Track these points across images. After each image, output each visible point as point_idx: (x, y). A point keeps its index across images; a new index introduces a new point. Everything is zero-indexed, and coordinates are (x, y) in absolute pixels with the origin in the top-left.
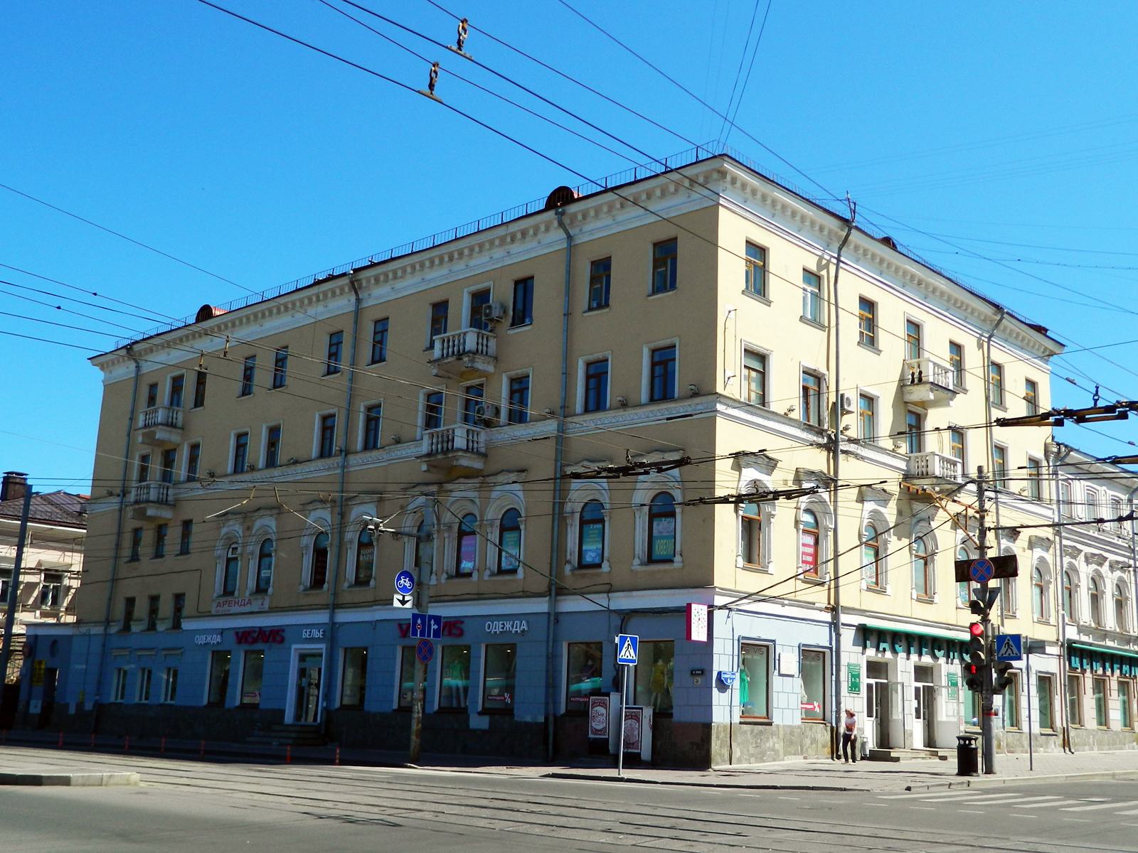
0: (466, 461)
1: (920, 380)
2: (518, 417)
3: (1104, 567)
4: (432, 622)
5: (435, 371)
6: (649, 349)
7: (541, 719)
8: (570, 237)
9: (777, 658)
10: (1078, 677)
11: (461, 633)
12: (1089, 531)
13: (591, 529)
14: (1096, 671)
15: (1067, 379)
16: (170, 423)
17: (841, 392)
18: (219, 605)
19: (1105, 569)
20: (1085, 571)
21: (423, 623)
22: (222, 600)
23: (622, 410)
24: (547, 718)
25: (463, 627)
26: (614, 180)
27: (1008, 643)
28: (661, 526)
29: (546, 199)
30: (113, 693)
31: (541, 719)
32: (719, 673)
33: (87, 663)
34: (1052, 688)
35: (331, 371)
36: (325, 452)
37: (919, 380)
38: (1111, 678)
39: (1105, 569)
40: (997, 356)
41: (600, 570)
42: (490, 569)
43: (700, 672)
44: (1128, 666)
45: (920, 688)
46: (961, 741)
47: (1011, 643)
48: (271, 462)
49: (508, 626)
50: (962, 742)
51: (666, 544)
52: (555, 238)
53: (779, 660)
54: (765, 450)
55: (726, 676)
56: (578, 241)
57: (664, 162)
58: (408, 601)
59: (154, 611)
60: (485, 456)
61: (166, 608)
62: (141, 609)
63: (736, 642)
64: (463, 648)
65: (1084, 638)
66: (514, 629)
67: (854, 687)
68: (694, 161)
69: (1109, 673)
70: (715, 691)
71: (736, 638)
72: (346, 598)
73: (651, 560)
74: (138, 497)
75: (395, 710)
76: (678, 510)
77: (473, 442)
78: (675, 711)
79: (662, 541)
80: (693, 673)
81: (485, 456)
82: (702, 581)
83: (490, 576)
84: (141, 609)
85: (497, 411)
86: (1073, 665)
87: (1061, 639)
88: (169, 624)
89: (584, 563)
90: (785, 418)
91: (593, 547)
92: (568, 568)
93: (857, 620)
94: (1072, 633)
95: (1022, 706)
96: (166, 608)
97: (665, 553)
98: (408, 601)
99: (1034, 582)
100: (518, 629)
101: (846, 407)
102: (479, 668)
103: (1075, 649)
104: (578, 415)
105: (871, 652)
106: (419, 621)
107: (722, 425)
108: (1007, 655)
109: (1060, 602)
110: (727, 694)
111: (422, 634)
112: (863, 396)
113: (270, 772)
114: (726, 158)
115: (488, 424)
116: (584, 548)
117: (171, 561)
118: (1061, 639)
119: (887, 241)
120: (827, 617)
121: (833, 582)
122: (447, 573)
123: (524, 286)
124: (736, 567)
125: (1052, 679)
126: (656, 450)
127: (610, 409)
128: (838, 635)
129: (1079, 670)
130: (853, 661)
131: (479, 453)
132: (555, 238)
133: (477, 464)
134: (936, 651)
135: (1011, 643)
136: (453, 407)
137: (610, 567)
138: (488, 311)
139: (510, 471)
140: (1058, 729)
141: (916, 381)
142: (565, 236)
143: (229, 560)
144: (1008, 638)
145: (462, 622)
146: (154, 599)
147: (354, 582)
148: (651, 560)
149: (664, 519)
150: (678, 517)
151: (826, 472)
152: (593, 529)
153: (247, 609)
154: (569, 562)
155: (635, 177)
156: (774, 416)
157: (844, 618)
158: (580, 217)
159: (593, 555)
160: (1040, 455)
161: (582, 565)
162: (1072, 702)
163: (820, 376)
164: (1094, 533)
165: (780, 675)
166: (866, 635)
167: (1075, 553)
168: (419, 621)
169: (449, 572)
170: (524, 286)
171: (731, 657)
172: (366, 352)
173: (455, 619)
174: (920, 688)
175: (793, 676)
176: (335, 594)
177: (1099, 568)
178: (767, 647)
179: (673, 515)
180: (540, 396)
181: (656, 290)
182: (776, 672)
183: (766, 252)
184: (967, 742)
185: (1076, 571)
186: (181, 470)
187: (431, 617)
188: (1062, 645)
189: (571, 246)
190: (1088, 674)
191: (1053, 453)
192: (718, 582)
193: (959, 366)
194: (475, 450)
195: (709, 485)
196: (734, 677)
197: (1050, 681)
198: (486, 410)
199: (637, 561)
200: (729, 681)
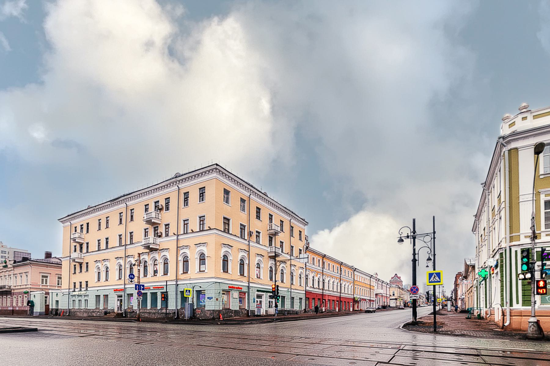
2: (167, 235)
4: (141, 286)
20: (310, 277)
21: (139, 287)
36: (120, 245)
48: (107, 248)
59: (81, 286)
61: (84, 285)
62: (78, 286)
76: (206, 258)
84: (78, 286)
88: (85, 289)
96: (84, 285)
106: (137, 286)
111: (139, 289)
115: (160, 236)
119: (477, 248)
120: (251, 285)
121: (386, 295)
143: (99, 273)
146: (81, 283)
160: (302, 249)
162: (292, 302)
168: (137, 286)
172: (124, 215)
180: (173, 229)
186: (84, 250)
187: (141, 285)
193: (282, 225)
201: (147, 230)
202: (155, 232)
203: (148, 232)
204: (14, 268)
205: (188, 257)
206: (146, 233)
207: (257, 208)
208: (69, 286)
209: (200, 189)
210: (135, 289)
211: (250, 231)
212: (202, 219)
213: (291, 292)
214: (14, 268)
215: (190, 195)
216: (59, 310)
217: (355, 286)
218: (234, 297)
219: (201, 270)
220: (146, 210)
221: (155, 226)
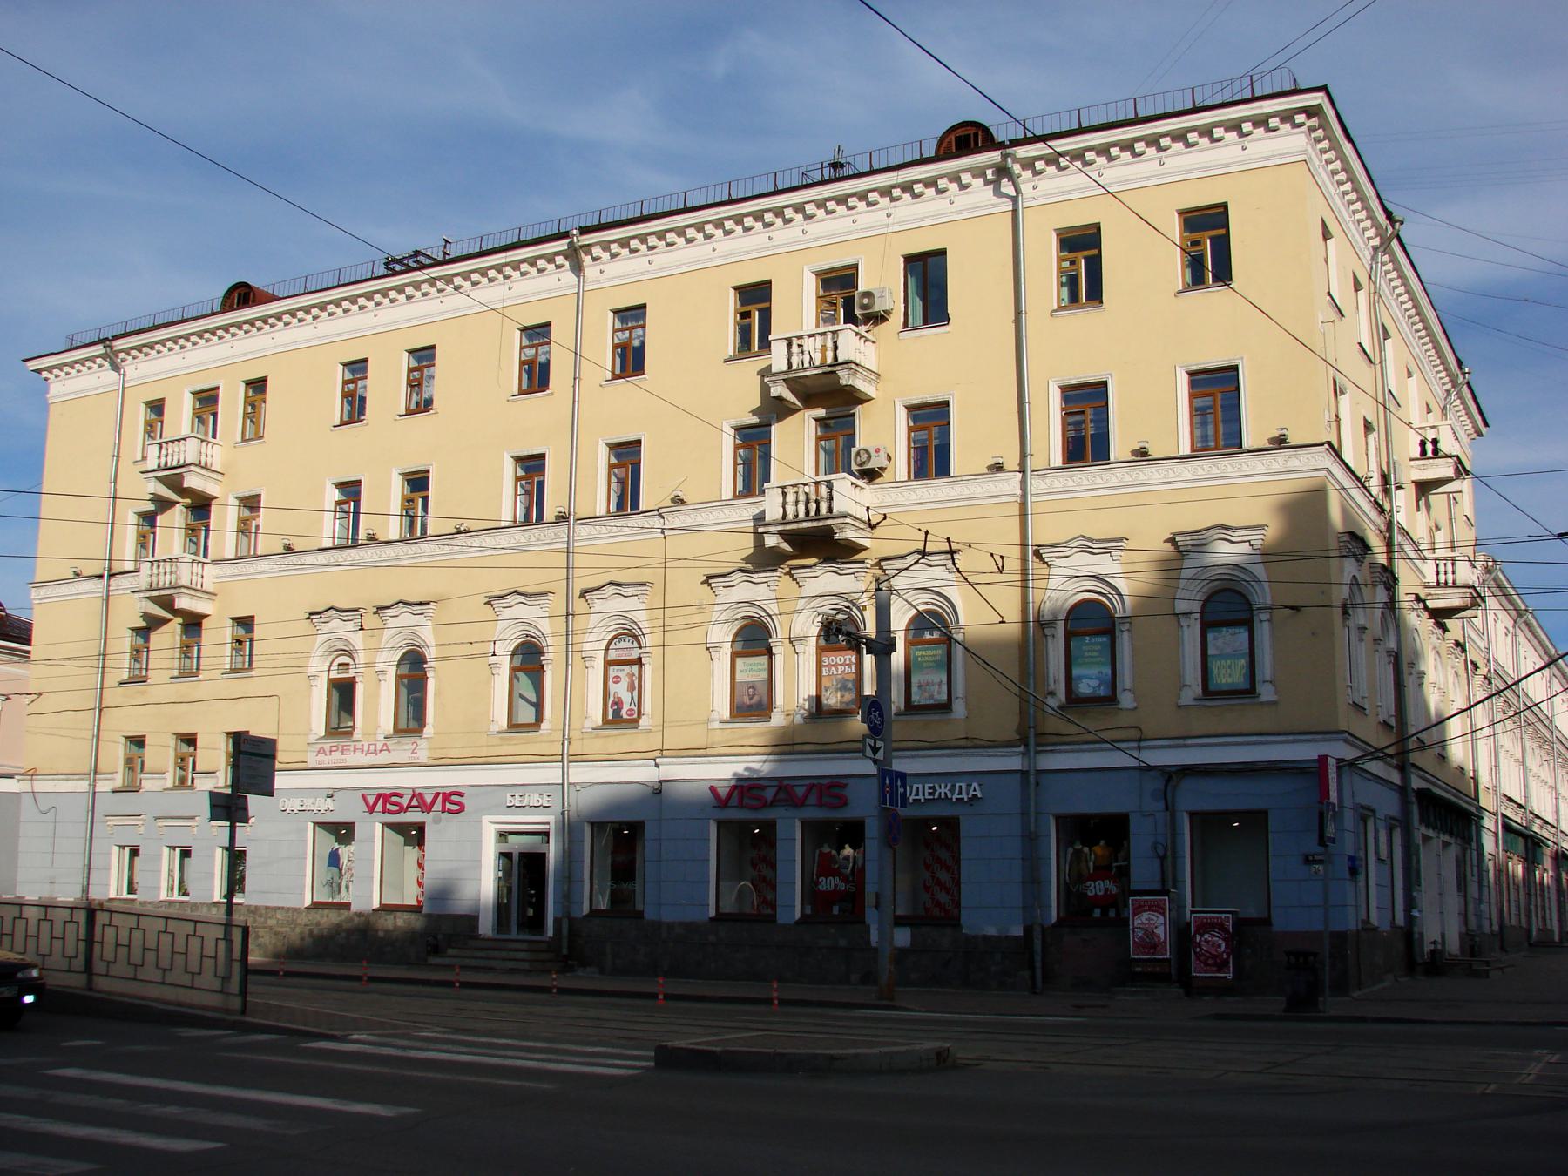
7: (1017, 931)
11: (844, 802)
13: (1086, 645)
15: (428, 603)
16: (203, 464)
18: (321, 751)
22: (327, 745)
24: (1028, 930)
25: (848, 792)
26: (490, 242)
28: (1220, 642)
29: (221, 300)
30: (164, 885)
31: (1017, 931)
33: (795, 818)
46: (1291, 957)
49: (943, 790)
50: (1293, 959)
51: (1230, 667)
57: (1022, 122)
58: (880, 748)
62: (161, 754)
64: (752, 826)
66: (956, 796)
68: (336, 284)
72: (1054, 724)
74: (155, 579)
75: (711, 919)
78: (1275, 920)
79: (1223, 662)
89: (1212, 688)
91: (1094, 671)
97: (1230, 680)
98: (880, 748)
100: (964, 795)
102: (708, 854)
116: (1076, 672)
117: (211, 681)
138: (866, 301)
145: (844, 786)
147: (903, 708)
149: (1224, 629)
152: (1091, 644)
153: (384, 758)
155: (730, 195)
159: (1094, 683)
173: (830, 780)
176: (565, 739)
184: (1301, 960)
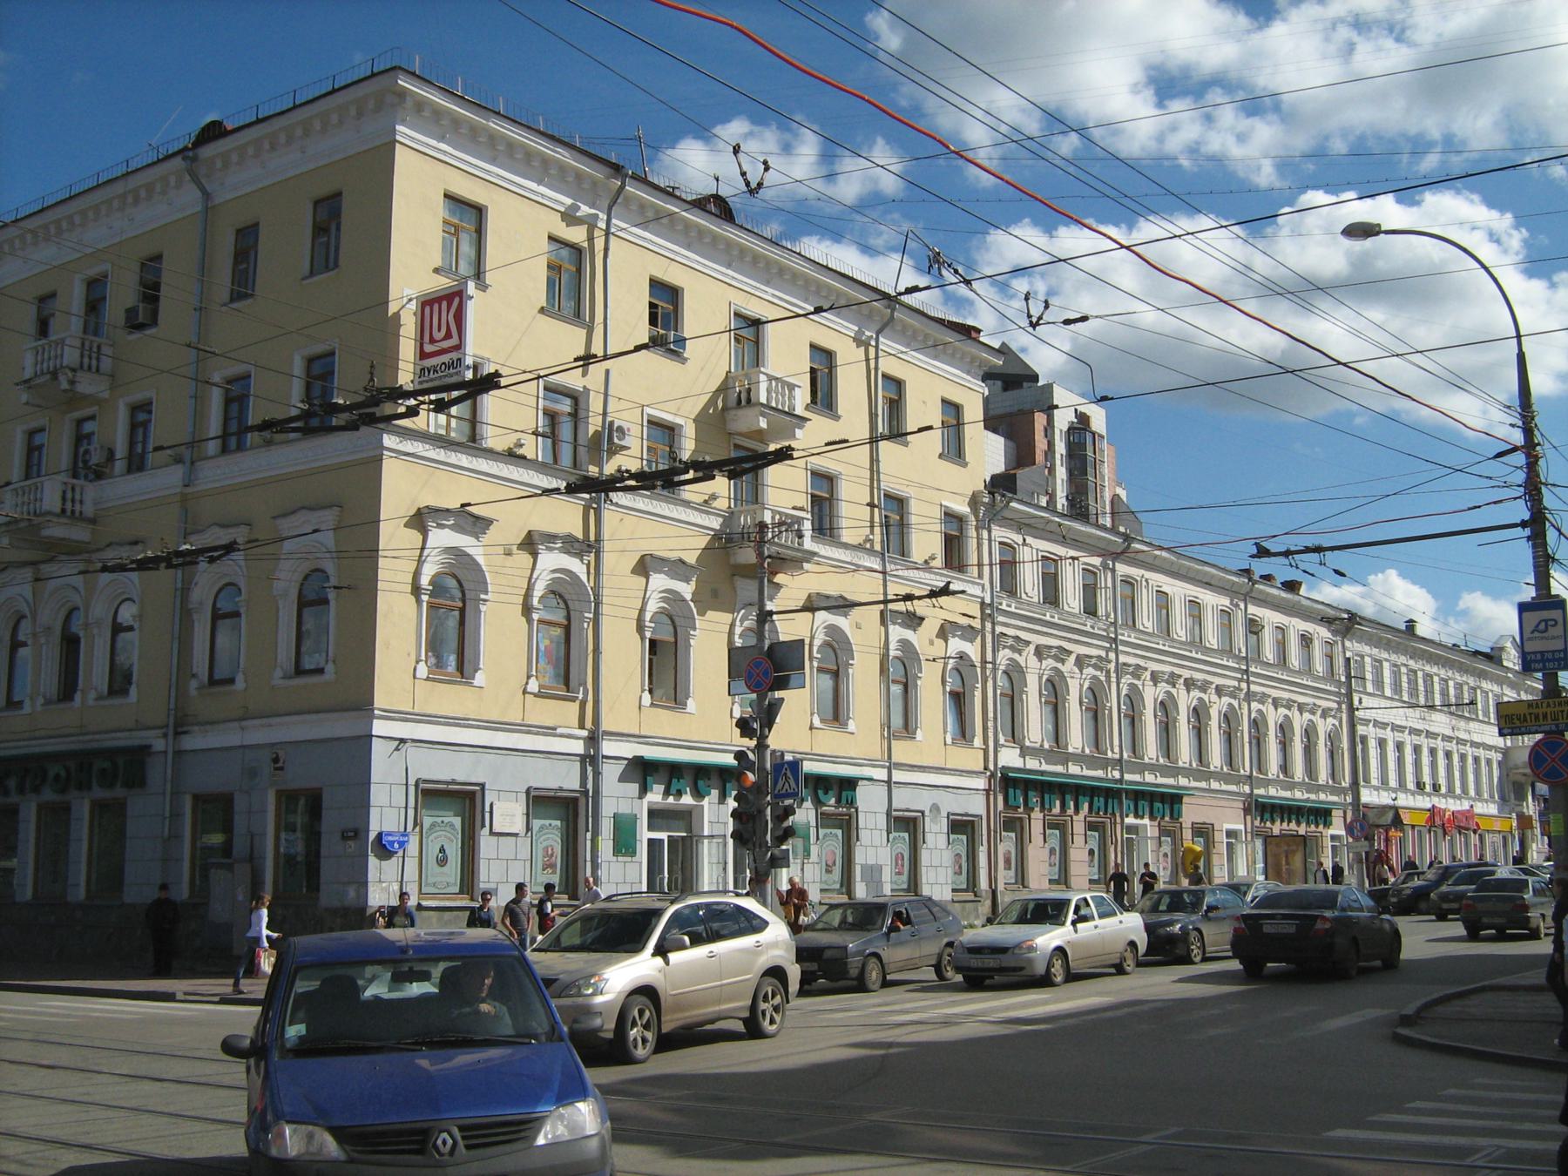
0: (57, 531)
1: (749, 401)
2: (136, 464)
3: (1067, 663)
5: (24, 397)
6: (302, 358)
8: (206, 195)
9: (487, 808)
10: (1021, 819)
12: (1045, 615)
14: (1050, 810)
17: (609, 419)
19: (1069, 666)
23: (263, 449)
27: (785, 774)
32: (380, 836)
34: (976, 837)
35: (145, 407)
37: (746, 400)
38: (1075, 818)
39: (1069, 666)
40: (888, 366)
41: (233, 688)
42: (96, 689)
43: (352, 834)
44: (1102, 799)
45: (663, 840)
47: (789, 774)
52: (188, 199)
53: (491, 813)
54: (469, 505)
55: (390, 838)
56: (218, 200)
60: (93, 521)
63: (412, 790)
65: (1032, 764)
67: (624, 844)
69: (1071, 811)
70: (373, 861)
71: (412, 781)
73: (299, 671)
76: (332, 595)
77: (73, 501)
80: (345, 838)
81: (93, 521)
82: (362, 704)
83: (96, 699)
85: (111, 455)
86: (1011, 801)
87: (991, 767)
90: (512, 456)
92: (194, 684)
93: (629, 750)
94: (1010, 758)
95: (981, 865)
99: (948, 689)
101: (616, 440)
103: (1015, 780)
104: (212, 458)
105: (655, 796)
107: (392, 472)
108: (784, 791)
109: (991, 715)
110: (394, 862)
112: (654, 423)
113: (115, 1012)
114: (400, 72)
118: (991, 767)
122: (44, 697)
123: (151, 267)
124: (415, 677)
125: (976, 824)
126: (303, 508)
127: (252, 448)
128: (597, 774)
129: (1021, 810)
130: (624, 808)
131: (82, 518)
132: (188, 199)
133: (80, 533)
134: (820, 792)
135: (789, 774)
136: (59, 450)
137: (246, 681)
139: (121, 544)
140: (984, 894)
141: (743, 403)
142: (199, 194)
144: (786, 766)
148: (299, 671)
150: (333, 603)
151: (580, 536)
154: (194, 676)
156: (490, 454)
157: (608, 747)
158: (219, 164)
160: (962, 508)
161: (213, 682)
163: (576, 395)
164: (1052, 617)
165: (492, 833)
166: (643, 771)
167: (1019, 645)
169: (48, 694)
170: (151, 267)
171: (403, 811)
174: (663, 840)
175: (516, 835)
177: (1059, 665)
178: (473, 793)
179: (326, 602)
180: (167, 427)
181: (158, 258)
182: (486, 830)
183: (484, 213)
185: (1021, 671)
188: (993, 775)
189: (209, 209)
190: (1037, 815)
191: (984, 504)
192: (380, 700)
194: (77, 514)
195: (374, 553)
196: (406, 839)
197: (973, 828)
198: (93, 453)
199: (278, 673)
200: (396, 845)
201: (38, 440)
202: (77, 447)
203: (45, 451)
204: (593, 513)
205: (328, 578)
206: (140, 431)
207: (656, 285)
208: (977, 790)
209: (317, 203)
210: (487, 787)
211: (611, 423)
212: (141, 413)
213: (889, 782)
214: (593, 513)
215: (265, 245)
216: (554, 1099)
217: (1361, 730)
218: (496, 828)
219: (217, 677)
220: (43, 328)
221: (77, 415)
